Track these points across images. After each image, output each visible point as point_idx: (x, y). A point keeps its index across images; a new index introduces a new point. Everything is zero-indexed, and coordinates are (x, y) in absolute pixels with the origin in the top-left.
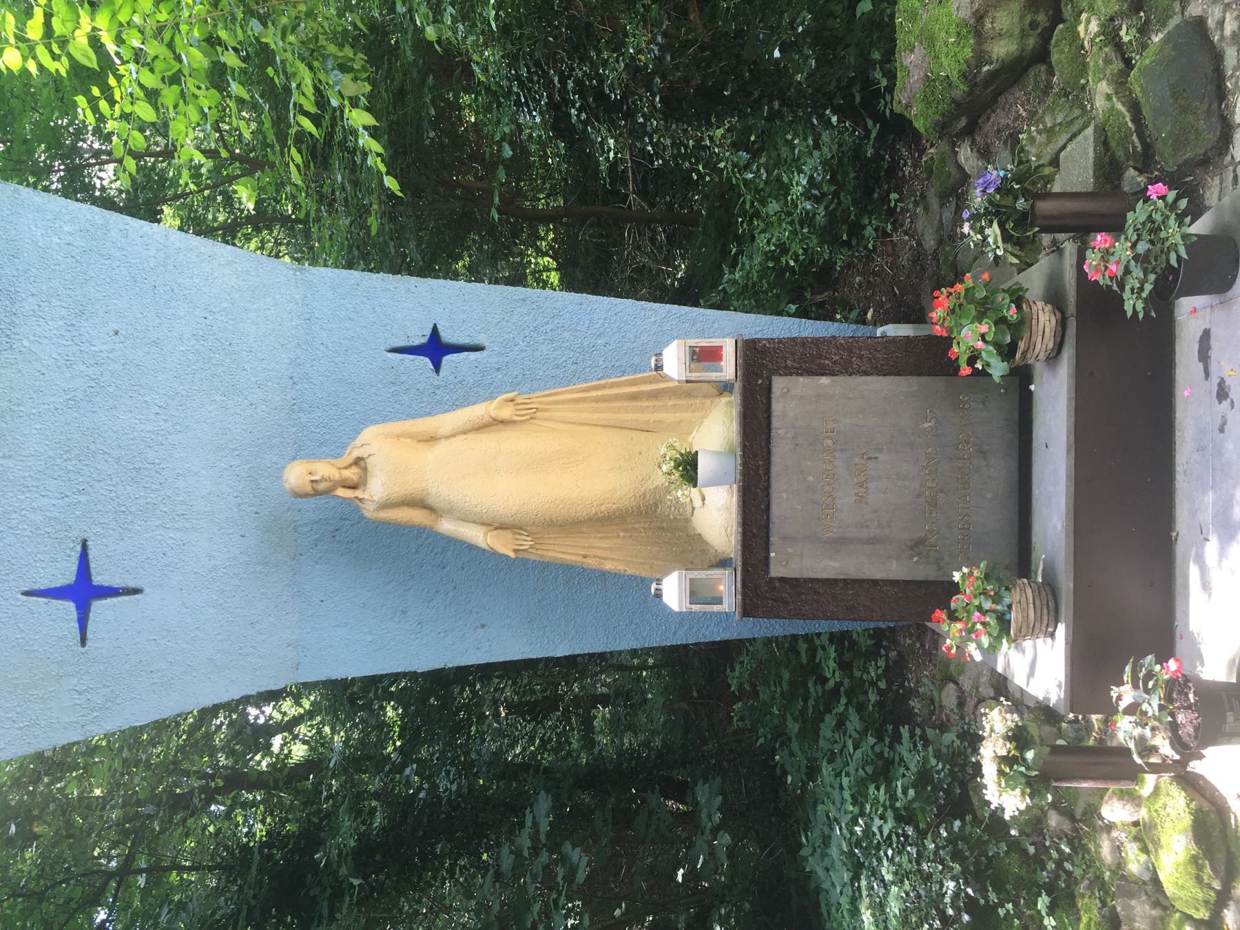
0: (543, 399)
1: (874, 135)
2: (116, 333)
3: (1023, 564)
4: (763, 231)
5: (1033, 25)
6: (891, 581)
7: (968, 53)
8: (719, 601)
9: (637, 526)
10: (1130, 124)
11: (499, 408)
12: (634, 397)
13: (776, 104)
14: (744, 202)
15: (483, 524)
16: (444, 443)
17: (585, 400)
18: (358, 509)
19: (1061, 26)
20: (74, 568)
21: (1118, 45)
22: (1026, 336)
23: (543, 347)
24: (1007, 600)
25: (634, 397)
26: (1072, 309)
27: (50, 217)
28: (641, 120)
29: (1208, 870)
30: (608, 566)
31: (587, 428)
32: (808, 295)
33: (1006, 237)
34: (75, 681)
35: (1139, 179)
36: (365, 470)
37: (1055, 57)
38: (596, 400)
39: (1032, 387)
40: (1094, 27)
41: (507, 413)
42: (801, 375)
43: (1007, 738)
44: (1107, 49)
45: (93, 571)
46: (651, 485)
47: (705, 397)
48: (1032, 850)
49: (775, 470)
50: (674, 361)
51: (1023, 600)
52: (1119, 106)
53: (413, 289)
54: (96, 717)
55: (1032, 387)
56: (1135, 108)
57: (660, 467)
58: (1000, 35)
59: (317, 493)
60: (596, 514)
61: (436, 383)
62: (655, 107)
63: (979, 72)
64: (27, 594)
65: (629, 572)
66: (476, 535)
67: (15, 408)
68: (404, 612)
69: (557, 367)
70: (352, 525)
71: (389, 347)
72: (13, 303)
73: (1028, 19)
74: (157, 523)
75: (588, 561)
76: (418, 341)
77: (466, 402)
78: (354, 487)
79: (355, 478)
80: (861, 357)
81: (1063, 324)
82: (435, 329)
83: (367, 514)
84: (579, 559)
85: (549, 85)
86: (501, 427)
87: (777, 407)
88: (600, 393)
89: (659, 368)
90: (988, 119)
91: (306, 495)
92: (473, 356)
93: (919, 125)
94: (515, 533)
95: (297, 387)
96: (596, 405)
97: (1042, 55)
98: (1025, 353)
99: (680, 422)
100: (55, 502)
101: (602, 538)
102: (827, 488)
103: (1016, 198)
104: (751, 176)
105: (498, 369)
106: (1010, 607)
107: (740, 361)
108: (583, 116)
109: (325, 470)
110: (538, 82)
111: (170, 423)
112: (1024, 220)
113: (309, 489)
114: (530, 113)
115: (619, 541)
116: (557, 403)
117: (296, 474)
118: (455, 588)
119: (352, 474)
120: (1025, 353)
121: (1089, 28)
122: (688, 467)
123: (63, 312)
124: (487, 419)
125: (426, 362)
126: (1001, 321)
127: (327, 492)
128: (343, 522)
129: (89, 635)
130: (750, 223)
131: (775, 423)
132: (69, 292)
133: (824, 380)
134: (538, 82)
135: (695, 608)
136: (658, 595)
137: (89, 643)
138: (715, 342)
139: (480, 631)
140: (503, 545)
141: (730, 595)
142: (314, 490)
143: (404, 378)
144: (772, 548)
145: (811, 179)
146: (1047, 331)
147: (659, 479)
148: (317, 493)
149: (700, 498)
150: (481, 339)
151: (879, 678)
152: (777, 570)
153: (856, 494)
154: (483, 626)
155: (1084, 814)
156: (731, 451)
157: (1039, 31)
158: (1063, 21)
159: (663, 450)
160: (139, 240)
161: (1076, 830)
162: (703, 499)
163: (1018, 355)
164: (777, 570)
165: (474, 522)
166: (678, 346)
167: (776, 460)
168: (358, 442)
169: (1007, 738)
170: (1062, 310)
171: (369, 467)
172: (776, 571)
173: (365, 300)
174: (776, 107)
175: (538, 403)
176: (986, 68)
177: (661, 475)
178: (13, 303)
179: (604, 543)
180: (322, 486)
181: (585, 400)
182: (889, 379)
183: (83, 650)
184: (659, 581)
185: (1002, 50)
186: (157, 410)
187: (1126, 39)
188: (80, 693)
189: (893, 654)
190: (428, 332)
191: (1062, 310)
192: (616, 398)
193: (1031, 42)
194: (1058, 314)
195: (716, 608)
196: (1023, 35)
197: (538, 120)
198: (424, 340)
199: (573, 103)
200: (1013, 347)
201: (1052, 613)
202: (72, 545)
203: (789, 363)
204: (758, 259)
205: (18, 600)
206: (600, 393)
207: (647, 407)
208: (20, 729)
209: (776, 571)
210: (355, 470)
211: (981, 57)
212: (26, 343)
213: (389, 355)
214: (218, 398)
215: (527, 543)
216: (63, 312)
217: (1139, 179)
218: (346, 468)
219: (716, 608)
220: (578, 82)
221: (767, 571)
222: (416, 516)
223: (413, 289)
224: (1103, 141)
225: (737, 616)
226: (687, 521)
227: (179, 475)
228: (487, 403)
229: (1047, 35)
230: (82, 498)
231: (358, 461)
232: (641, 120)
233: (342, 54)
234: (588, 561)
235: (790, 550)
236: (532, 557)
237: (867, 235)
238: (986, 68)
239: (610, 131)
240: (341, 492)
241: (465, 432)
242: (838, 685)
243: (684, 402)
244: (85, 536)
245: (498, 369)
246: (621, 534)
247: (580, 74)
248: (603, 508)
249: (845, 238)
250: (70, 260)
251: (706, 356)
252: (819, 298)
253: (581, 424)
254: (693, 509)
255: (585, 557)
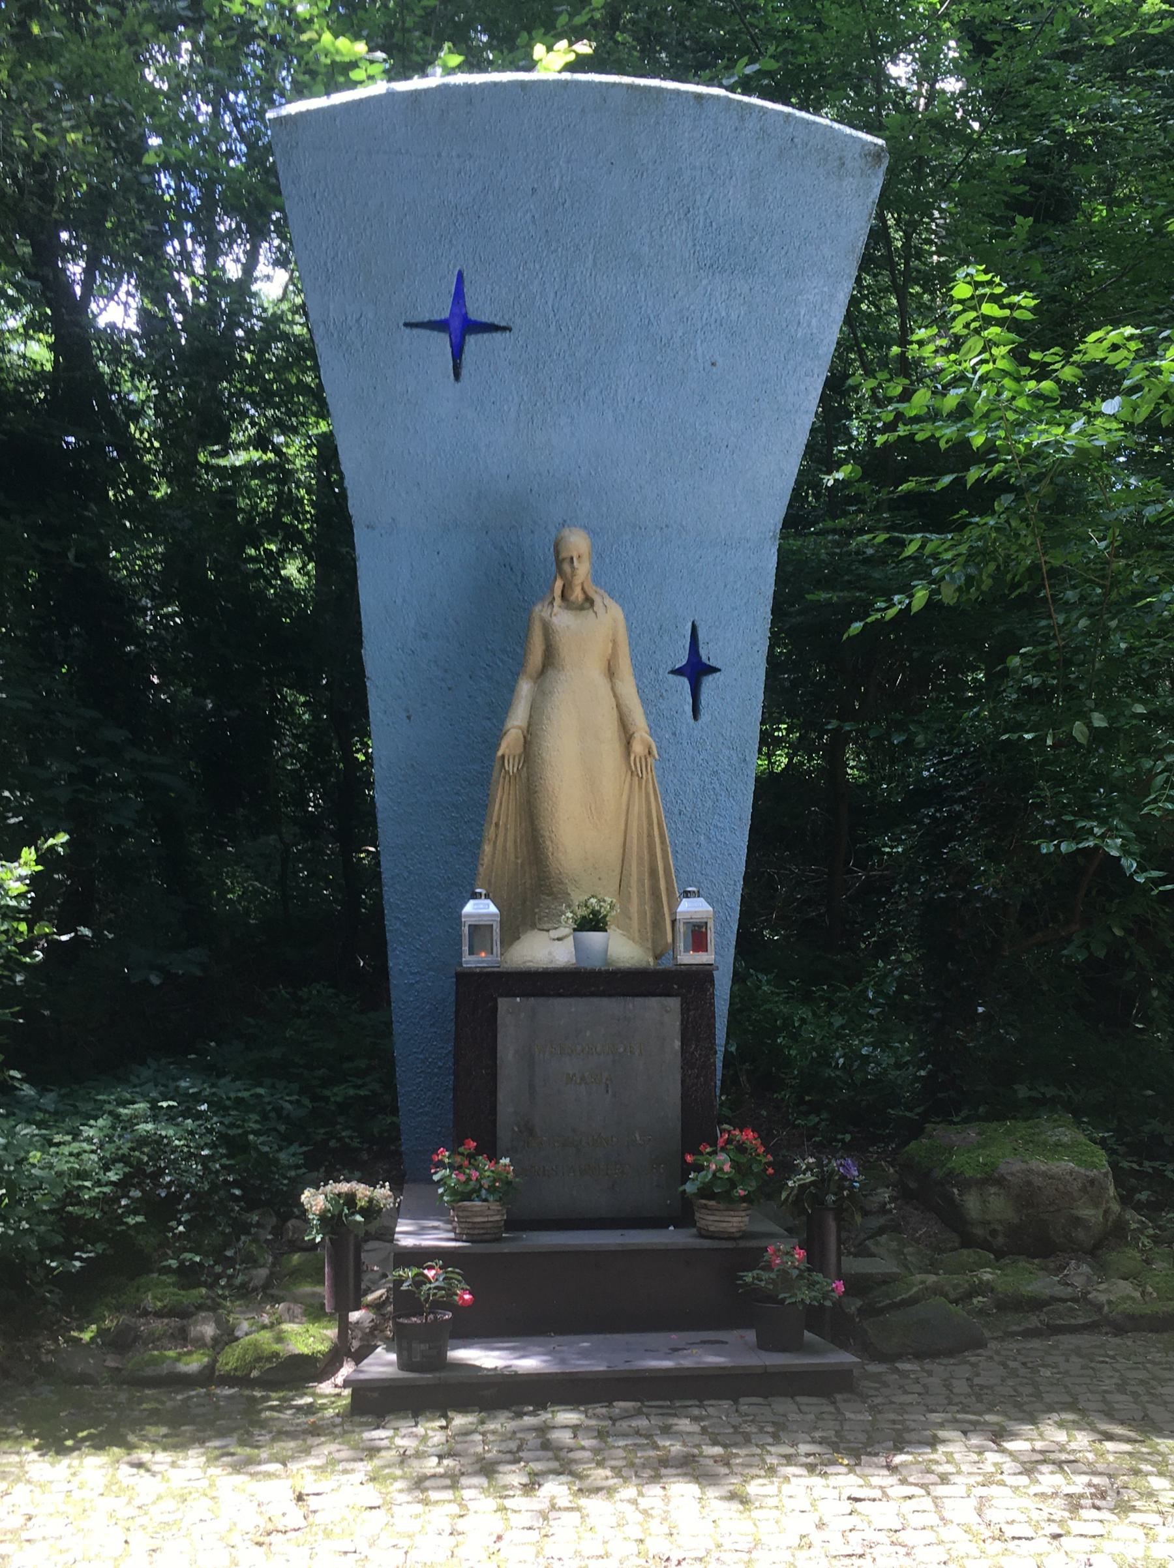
0: (651, 785)
1: (908, 1114)
2: (713, 364)
3: (515, 1224)
4: (814, 1014)
5: (994, 1233)
6: (495, 1107)
7: (969, 1173)
8: (471, 953)
9: (527, 875)
10: (899, 1298)
11: (643, 741)
12: (653, 872)
13: (938, 1015)
14: (844, 990)
15: (529, 725)
16: (609, 686)
17: (650, 824)
18: (542, 599)
19: (992, 1256)
20: (484, 319)
21: (970, 1295)
22: (721, 1206)
23: (696, 780)
24: (491, 1199)
25: (653, 872)
26: (743, 1244)
27: (825, 307)
28: (923, 879)
29: (268, 1366)
30: (487, 848)
31: (622, 827)
32: (747, 1066)
33: (803, 1187)
34: (370, 315)
35: (853, 1308)
36: (581, 608)
37: (965, 1251)
38: (650, 836)
39: (672, 1228)
40: (987, 1277)
41: (638, 748)
42: (682, 1024)
43: (371, 1200)
44: (966, 1286)
45: (479, 336)
46: (570, 889)
47: (653, 942)
48: (229, 1253)
49: (596, 1001)
50: (692, 908)
51: (491, 1212)
52: (915, 1289)
53: (756, 648)
54: (332, 335)
55: (672, 1228)
56: (914, 1301)
57: (593, 896)
58: (984, 1202)
59: (559, 562)
60: (542, 836)
61: (661, 671)
62: (935, 893)
63: (953, 1186)
64: (460, 276)
65: (481, 870)
66: (518, 718)
67: (642, 270)
68: (425, 636)
69: (677, 795)
70: (516, 584)
71: (697, 624)
72: (743, 271)
73: (1000, 1228)
74: (525, 398)
75: (493, 828)
76: (703, 653)
77: (645, 702)
78: (563, 596)
79: (573, 598)
80: (698, 1077)
81: (730, 1237)
82: (715, 670)
83: (538, 608)
84: (495, 819)
85: (958, 786)
86: (625, 742)
87: (653, 1002)
88: (657, 840)
89: (687, 894)
90: (916, 1209)
91: (557, 552)
92: (689, 709)
93: (913, 1145)
94: (520, 756)
95: (658, 531)
96: (645, 836)
97: (968, 1241)
98: (705, 1207)
99: (630, 918)
100: (550, 304)
101: (515, 842)
102: (579, 1048)
103: (835, 1194)
104: (871, 995)
105: (674, 734)
106: (485, 1200)
107: (694, 968)
108: (927, 821)
109: (583, 570)
110: (961, 775)
111: (624, 411)
112: (818, 1200)
113: (564, 554)
114: (933, 765)
115: (512, 857)
116: (647, 795)
117: (578, 543)
118: (450, 689)
119: (577, 595)
120: (705, 1207)
121: (987, 1275)
122: (593, 922)
123: (734, 317)
124: (632, 729)
125: (682, 660)
126: (733, 1185)
127: (560, 571)
128: (519, 575)
129: (415, 331)
130: (822, 998)
131: (639, 1001)
132: (753, 322)
133: (677, 1044)
134: (961, 775)
135: (466, 930)
136: (475, 896)
137: (408, 331)
138: (711, 946)
139: (405, 714)
140: (510, 744)
141: (479, 962)
142: (564, 559)
143: (666, 638)
144: (524, 999)
145: (866, 1059)
146: (725, 1225)
147: (577, 897)
148: (559, 562)
149: (560, 936)
150: (705, 717)
151: (340, 1140)
152: (504, 1004)
153: (574, 1075)
154: (409, 717)
155: (272, 1296)
156: (606, 961)
157: (989, 1238)
158: (997, 1259)
159: (609, 900)
160: (803, 387)
161: (255, 1289)
162: (559, 939)
163: (704, 1201)
164: (504, 1004)
165: (531, 716)
166: (708, 912)
167: (605, 1002)
168: (608, 601)
169: (371, 1200)
170: (741, 1238)
171: (584, 612)
172: (503, 1004)
173: (745, 600)
174: (935, 1015)
175: (647, 781)
176: (956, 1191)
177: (580, 897)
178: (743, 271)
179: (510, 844)
180: (566, 567)
181: (650, 824)
182: (679, 1102)
183: (401, 324)
184: (487, 896)
185: (972, 1204)
186: (637, 399)
187: (975, 1301)
188: (357, 321)
189: (365, 1157)
190: (713, 663)
191: (741, 1238)
192: (653, 856)
193: (979, 1231)
194: (738, 1235)
195: (466, 948)
196: (985, 1223)
197: (926, 774)
198: (704, 659)
199: (941, 811)
200: (712, 1196)
201: (479, 1238)
202: (507, 318)
203: (692, 1013)
204: (785, 1009)
205: (454, 267)
206: (657, 840)
207: (643, 886)
208: (325, 264)
209: (503, 1004)
210: (581, 597)
211: (966, 1185)
212: (704, 282)
213: (690, 624)
214: (648, 456)
215: (511, 767)
216: (734, 317)
217: (853, 1308)
218: (583, 589)
219: (466, 948)
220: (959, 816)
221: (502, 995)
222: (536, 657)
223: (756, 648)
224: (887, 1280)
225: (459, 969)
226: (533, 926)
227: (573, 418)
228: (647, 729)
229: (986, 1246)
230: (553, 329)
231: (589, 601)
232: (923, 879)
233: (984, 578)
234: (493, 828)
235: (523, 1015)
236: (495, 774)
237: (811, 1117)
238: (956, 1191)
239: (912, 847)
240: (559, 584)
241: (618, 706)
242: (326, 1099)
243: (648, 921)
244: (515, 330)
245: (674, 734)
246: (519, 861)
247: (968, 817)
248: (548, 843)
249: (807, 1098)
250: (784, 325)
251: (698, 936)
252: (743, 1079)
253: (626, 825)
254: (548, 931)
255: (497, 825)
